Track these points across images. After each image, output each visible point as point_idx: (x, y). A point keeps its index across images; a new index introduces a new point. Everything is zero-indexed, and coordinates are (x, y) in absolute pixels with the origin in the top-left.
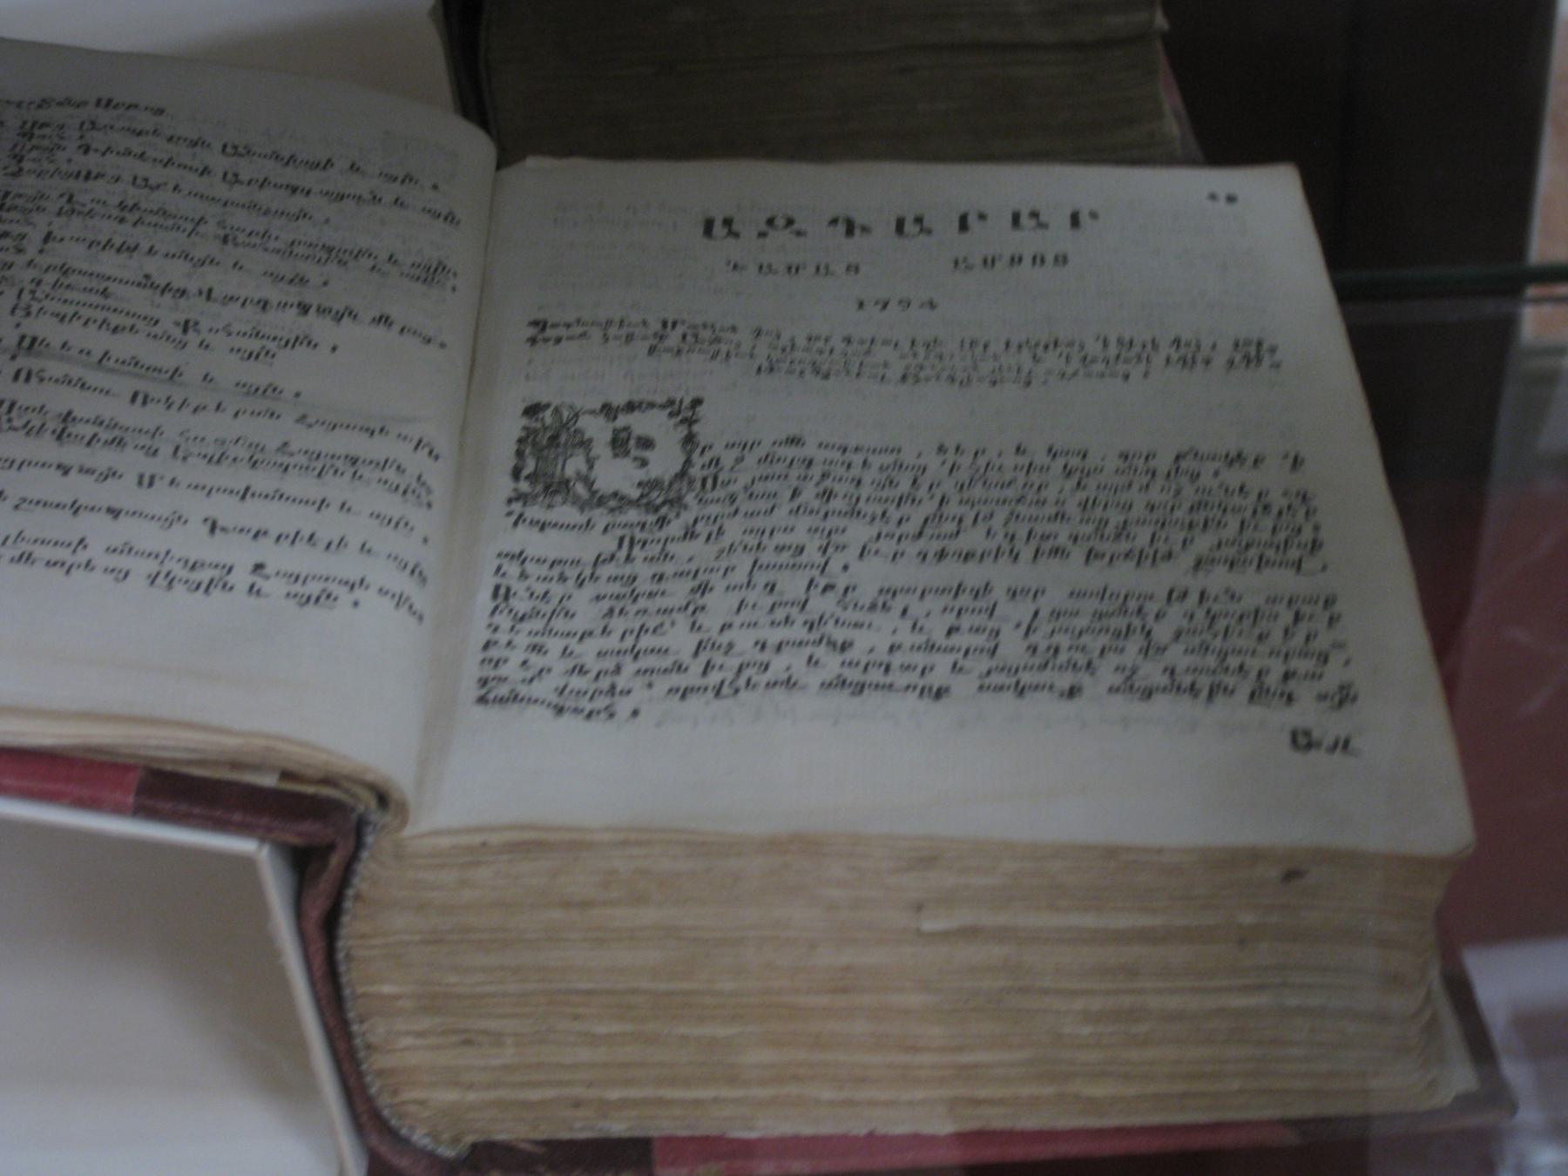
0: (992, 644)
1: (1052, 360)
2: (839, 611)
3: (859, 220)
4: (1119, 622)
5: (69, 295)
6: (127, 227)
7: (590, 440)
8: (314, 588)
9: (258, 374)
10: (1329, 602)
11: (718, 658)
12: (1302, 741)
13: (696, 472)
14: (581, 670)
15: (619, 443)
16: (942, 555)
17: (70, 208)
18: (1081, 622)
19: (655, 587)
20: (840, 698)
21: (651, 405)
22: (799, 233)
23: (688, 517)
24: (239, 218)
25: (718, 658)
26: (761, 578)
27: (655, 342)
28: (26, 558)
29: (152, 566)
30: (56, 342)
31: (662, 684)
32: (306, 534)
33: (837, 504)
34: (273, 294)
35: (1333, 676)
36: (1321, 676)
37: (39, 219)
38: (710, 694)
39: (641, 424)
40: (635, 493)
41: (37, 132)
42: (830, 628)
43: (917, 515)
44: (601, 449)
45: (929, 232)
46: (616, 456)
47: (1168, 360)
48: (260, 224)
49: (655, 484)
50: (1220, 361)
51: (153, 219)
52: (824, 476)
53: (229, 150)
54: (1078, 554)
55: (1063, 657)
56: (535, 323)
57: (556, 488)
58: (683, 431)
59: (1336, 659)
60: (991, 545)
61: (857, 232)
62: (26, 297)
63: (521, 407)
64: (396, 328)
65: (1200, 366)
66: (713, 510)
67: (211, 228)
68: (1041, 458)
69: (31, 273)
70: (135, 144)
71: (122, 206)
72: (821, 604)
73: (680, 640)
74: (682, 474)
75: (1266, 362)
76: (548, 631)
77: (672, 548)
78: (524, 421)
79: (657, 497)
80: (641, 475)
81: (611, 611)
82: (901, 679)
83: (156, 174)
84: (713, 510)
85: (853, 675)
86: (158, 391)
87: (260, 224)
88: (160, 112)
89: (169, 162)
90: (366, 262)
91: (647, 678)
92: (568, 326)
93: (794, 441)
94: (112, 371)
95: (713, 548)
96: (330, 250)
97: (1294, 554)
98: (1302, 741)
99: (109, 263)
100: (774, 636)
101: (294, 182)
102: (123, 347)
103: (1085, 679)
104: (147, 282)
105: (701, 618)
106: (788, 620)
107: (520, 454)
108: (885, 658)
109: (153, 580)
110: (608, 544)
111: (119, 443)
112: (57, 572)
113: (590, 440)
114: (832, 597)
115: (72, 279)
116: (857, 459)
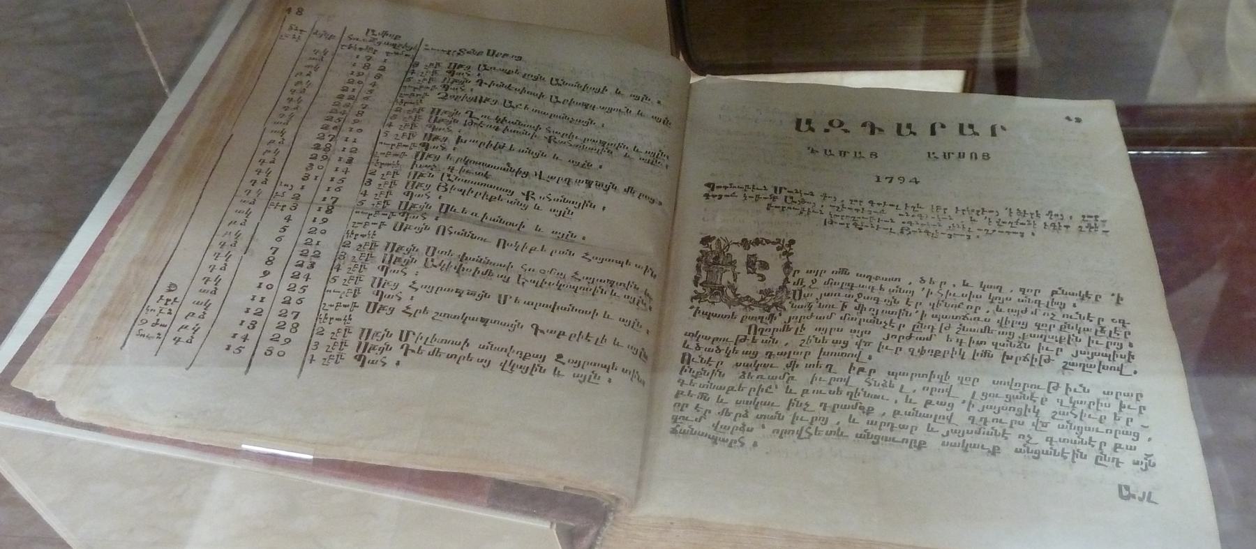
4: (1020, 404)
5: (468, 177)
6: (499, 133)
9: (563, 226)
10: (1139, 396)
11: (800, 414)
12: (1125, 493)
13: (790, 287)
15: (751, 264)
16: (922, 352)
17: (472, 121)
19: (767, 361)
21: (768, 242)
22: (846, 131)
23: (785, 316)
24: (559, 126)
25: (800, 414)
26: (825, 361)
28: (436, 353)
29: (502, 357)
31: (771, 425)
33: (866, 315)
34: (573, 176)
35: (1143, 448)
37: (454, 127)
38: (796, 436)
39: (763, 252)
40: (758, 297)
41: (457, 71)
42: (861, 398)
48: (568, 128)
49: (767, 292)
50: (1074, 227)
51: (513, 127)
52: (859, 295)
54: (997, 355)
55: (988, 428)
56: (708, 185)
57: (717, 291)
62: (445, 178)
63: (700, 238)
64: (636, 195)
66: (799, 313)
67: (542, 133)
68: (977, 291)
69: (449, 163)
70: (506, 79)
71: (497, 119)
72: (858, 381)
74: (783, 288)
75: (1101, 229)
76: (712, 386)
77: (777, 336)
78: (701, 247)
79: (770, 301)
80: (761, 286)
83: (516, 98)
84: (799, 313)
86: (511, 239)
87: (568, 128)
88: (520, 58)
90: (622, 151)
93: (844, 271)
94: (489, 226)
95: (798, 339)
96: (603, 143)
97: (1119, 361)
98: (1125, 493)
99: (489, 156)
100: (831, 400)
102: (494, 210)
104: (508, 168)
106: (839, 391)
107: (698, 268)
108: (891, 420)
110: (742, 330)
111: (488, 273)
114: (863, 376)
116: (877, 284)
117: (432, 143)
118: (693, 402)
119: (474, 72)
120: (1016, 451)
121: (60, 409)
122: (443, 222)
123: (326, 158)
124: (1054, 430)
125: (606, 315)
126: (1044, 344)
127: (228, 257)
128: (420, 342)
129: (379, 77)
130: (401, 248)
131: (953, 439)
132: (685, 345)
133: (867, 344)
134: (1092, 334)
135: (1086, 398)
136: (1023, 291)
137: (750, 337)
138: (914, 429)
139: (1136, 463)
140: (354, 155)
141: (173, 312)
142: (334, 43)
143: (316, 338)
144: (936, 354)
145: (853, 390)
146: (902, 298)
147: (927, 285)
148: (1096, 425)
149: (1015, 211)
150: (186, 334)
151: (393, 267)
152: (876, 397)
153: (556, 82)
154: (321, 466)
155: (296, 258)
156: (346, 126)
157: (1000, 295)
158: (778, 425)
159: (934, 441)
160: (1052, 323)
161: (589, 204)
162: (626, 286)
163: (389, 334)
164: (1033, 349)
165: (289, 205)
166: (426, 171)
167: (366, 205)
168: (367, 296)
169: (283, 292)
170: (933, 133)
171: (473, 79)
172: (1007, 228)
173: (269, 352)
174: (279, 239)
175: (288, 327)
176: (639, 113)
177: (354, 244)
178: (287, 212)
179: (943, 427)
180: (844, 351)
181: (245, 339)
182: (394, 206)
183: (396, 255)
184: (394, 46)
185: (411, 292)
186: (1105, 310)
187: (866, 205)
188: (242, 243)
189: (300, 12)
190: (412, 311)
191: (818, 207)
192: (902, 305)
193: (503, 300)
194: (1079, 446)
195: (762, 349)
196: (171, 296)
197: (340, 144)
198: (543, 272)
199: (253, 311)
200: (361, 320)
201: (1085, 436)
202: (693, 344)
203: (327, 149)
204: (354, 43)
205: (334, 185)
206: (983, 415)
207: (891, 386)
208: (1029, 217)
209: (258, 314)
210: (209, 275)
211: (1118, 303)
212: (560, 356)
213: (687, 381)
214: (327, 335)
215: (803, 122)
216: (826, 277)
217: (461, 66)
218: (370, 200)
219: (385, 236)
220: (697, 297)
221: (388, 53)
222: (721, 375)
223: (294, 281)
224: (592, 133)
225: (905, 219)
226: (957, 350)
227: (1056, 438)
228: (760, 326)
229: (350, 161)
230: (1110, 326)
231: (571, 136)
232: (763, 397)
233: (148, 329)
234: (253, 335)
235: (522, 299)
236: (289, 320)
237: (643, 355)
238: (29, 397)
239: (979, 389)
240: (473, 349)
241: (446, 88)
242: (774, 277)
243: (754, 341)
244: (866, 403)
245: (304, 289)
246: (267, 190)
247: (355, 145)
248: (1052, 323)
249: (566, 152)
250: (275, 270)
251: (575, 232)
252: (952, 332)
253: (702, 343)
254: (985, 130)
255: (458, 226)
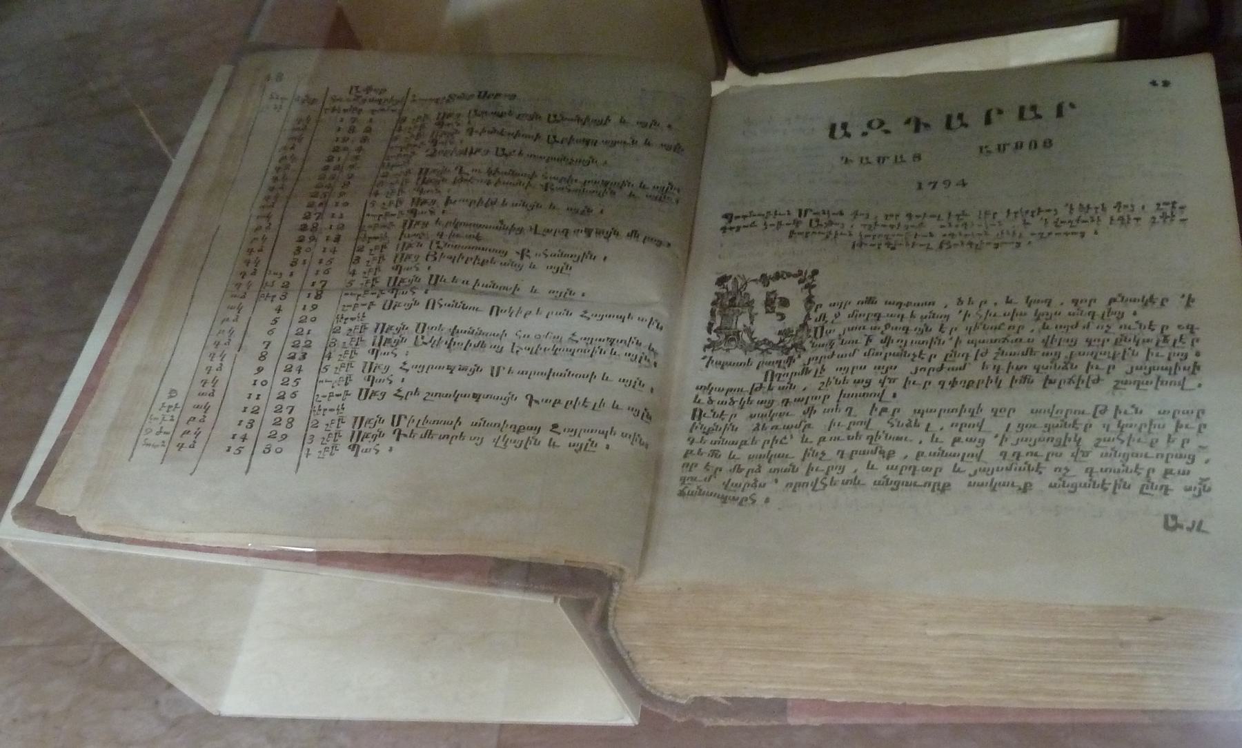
0: (978, 451)
1: (1036, 224)
2: (887, 427)
3: (924, 120)
4: (1059, 434)
7: (753, 301)
8: (584, 439)
12: (1171, 523)
13: (811, 323)
14: (738, 469)
15: (769, 304)
16: (953, 383)
17: (462, 179)
18: (1035, 434)
19: (784, 409)
20: (885, 492)
21: (789, 275)
22: (887, 132)
23: (805, 357)
25: (816, 464)
26: (845, 404)
27: (793, 227)
28: (429, 434)
29: (495, 433)
30: (448, 277)
31: (784, 479)
32: (581, 400)
33: (893, 348)
34: (572, 226)
35: (1198, 470)
36: (1189, 473)
38: (810, 488)
40: (776, 339)
43: (941, 352)
44: (759, 308)
45: (966, 125)
46: (767, 312)
47: (1112, 219)
50: (1146, 218)
51: (506, 179)
52: (887, 326)
53: (552, 118)
54: (1038, 379)
55: (1021, 463)
56: (725, 216)
57: (732, 337)
58: (805, 294)
59: (1200, 458)
60: (983, 375)
61: (922, 127)
62: (435, 245)
63: (715, 278)
64: (641, 238)
65: (1133, 222)
66: (821, 352)
68: (1022, 307)
69: (438, 229)
71: (489, 172)
72: (879, 423)
73: (795, 448)
74: (804, 326)
75: (1178, 218)
76: (723, 442)
77: (795, 380)
78: (717, 289)
80: (780, 326)
81: (757, 428)
82: (921, 478)
84: (821, 352)
85: (893, 476)
86: (505, 304)
89: (516, 135)
90: (627, 190)
91: (775, 476)
92: (744, 217)
93: (871, 301)
94: (481, 293)
96: (606, 184)
98: (1171, 523)
99: (482, 216)
100: (848, 446)
101: (587, 137)
103: (1034, 478)
104: (501, 226)
105: (808, 433)
107: (713, 313)
108: (914, 463)
109: (496, 442)
110: (759, 377)
111: (482, 345)
112: (445, 442)
113: (753, 301)
115: (460, 231)
116: (907, 312)
117: (419, 209)
118: (702, 461)
119: (464, 120)
120: (1051, 486)
121: (80, 522)
122: (434, 294)
123: (313, 239)
124: (1096, 460)
125: (605, 378)
126: (1094, 363)
127: (222, 357)
128: (413, 426)
129: (364, 140)
130: (391, 328)
131: (982, 478)
132: (697, 400)
133: (892, 381)
134: (1152, 345)
135: (1137, 419)
136: (1075, 302)
137: (766, 385)
138: (938, 470)
139: (1188, 489)
140: (340, 233)
141: (176, 418)
142: (316, 107)
143: (311, 431)
144: (969, 384)
145: (874, 434)
146: (935, 325)
147: (964, 307)
148: (1147, 449)
149: (1076, 206)
150: (188, 440)
151: (383, 349)
152: (899, 439)
153: (555, 119)
154: (325, 558)
155: (289, 350)
156: (332, 201)
157: (1049, 310)
158: (792, 478)
159: (959, 482)
160: (1107, 336)
161: (589, 255)
162: (627, 343)
163: (381, 420)
164: (1081, 370)
165: (279, 295)
166: (415, 239)
167: (355, 285)
168: (359, 382)
169: (278, 388)
170: (988, 121)
171: (463, 129)
172: (1065, 228)
173: (268, 450)
174: (270, 332)
175: (284, 423)
176: (647, 143)
177: (344, 328)
178: (277, 303)
179: (970, 466)
180: (866, 390)
181: (244, 439)
182: (383, 283)
183: (386, 336)
184: (380, 101)
185: (402, 374)
186: (1173, 316)
187: (903, 219)
188: (236, 340)
189: (280, 77)
190: (403, 394)
191: (847, 227)
192: (935, 332)
193: (495, 372)
194: (1123, 475)
195: (778, 396)
196: (173, 402)
197: (325, 222)
198: (538, 337)
199: (249, 410)
200: (355, 407)
201: (1132, 463)
202: (704, 398)
203: (314, 228)
204: (337, 104)
205: (323, 267)
206: (1016, 449)
207: (917, 425)
208: (1092, 212)
209: (255, 412)
210: (205, 377)
211: (1188, 305)
212: (555, 426)
213: (698, 439)
214: (322, 426)
215: (838, 127)
216: (849, 310)
217: (450, 115)
218: (359, 280)
219: (374, 317)
220: (711, 345)
221: (373, 112)
222: (734, 429)
223: (287, 375)
224: (594, 173)
225: (947, 231)
226: (993, 378)
227: (1097, 469)
228: (777, 371)
229: (337, 239)
230: (1174, 333)
231: (570, 180)
232: (777, 449)
233: (152, 438)
234: (252, 434)
235: (516, 370)
236: (285, 415)
237: (646, 416)
238: (52, 514)
239: (1014, 420)
240: (465, 426)
241: (435, 142)
242: (795, 314)
243: (770, 388)
244: (887, 446)
245: (297, 381)
246: (257, 280)
247: (342, 221)
248: (1107, 336)
249: (562, 199)
250: (269, 365)
251: (574, 289)
252: (989, 359)
253: (716, 396)
254: (1048, 111)
255: (448, 297)
